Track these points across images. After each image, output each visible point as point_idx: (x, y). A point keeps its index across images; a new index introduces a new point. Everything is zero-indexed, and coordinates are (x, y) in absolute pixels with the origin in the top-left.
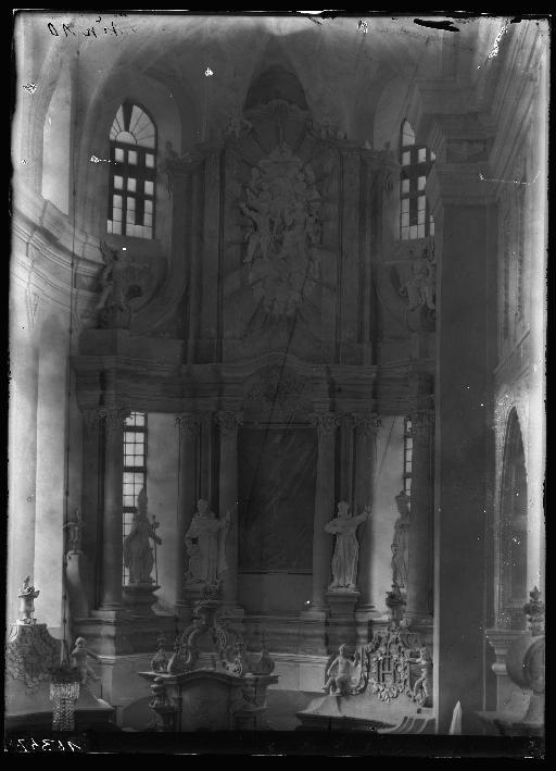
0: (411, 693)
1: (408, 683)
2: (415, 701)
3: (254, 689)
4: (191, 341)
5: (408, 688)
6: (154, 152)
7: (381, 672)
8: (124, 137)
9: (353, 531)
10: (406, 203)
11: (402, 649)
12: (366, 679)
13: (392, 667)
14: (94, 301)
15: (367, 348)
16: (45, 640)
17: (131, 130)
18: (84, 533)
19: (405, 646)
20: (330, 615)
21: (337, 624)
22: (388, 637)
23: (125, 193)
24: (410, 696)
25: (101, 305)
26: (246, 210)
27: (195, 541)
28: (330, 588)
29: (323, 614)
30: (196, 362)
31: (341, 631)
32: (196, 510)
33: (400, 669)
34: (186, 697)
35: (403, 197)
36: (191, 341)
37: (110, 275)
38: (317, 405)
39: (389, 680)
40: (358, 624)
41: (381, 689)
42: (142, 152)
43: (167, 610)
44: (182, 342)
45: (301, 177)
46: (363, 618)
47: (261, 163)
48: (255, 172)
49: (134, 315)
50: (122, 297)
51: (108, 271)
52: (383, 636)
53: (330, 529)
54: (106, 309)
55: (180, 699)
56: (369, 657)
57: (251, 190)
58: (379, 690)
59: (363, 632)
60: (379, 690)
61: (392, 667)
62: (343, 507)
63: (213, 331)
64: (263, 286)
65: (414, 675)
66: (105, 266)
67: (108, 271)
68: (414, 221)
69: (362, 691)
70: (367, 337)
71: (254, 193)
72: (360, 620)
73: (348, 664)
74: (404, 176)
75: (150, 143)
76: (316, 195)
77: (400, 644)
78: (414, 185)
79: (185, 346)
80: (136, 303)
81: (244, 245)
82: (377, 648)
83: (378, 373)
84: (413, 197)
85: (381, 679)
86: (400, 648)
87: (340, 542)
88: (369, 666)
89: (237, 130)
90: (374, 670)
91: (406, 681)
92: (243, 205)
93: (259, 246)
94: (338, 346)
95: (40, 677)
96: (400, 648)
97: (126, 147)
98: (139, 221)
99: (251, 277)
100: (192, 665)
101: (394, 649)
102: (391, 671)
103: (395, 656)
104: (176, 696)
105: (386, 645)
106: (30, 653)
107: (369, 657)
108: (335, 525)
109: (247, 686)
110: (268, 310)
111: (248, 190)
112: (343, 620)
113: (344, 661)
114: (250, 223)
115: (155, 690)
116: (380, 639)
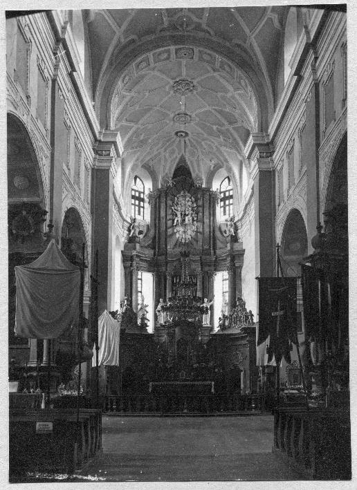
8: (135, 188)
15: (212, 251)
23: (135, 205)
39: (238, 322)
66: (131, 224)
74: (221, 201)
80: (141, 236)
81: (173, 220)
97: (135, 191)
98: (139, 214)
99: (175, 231)
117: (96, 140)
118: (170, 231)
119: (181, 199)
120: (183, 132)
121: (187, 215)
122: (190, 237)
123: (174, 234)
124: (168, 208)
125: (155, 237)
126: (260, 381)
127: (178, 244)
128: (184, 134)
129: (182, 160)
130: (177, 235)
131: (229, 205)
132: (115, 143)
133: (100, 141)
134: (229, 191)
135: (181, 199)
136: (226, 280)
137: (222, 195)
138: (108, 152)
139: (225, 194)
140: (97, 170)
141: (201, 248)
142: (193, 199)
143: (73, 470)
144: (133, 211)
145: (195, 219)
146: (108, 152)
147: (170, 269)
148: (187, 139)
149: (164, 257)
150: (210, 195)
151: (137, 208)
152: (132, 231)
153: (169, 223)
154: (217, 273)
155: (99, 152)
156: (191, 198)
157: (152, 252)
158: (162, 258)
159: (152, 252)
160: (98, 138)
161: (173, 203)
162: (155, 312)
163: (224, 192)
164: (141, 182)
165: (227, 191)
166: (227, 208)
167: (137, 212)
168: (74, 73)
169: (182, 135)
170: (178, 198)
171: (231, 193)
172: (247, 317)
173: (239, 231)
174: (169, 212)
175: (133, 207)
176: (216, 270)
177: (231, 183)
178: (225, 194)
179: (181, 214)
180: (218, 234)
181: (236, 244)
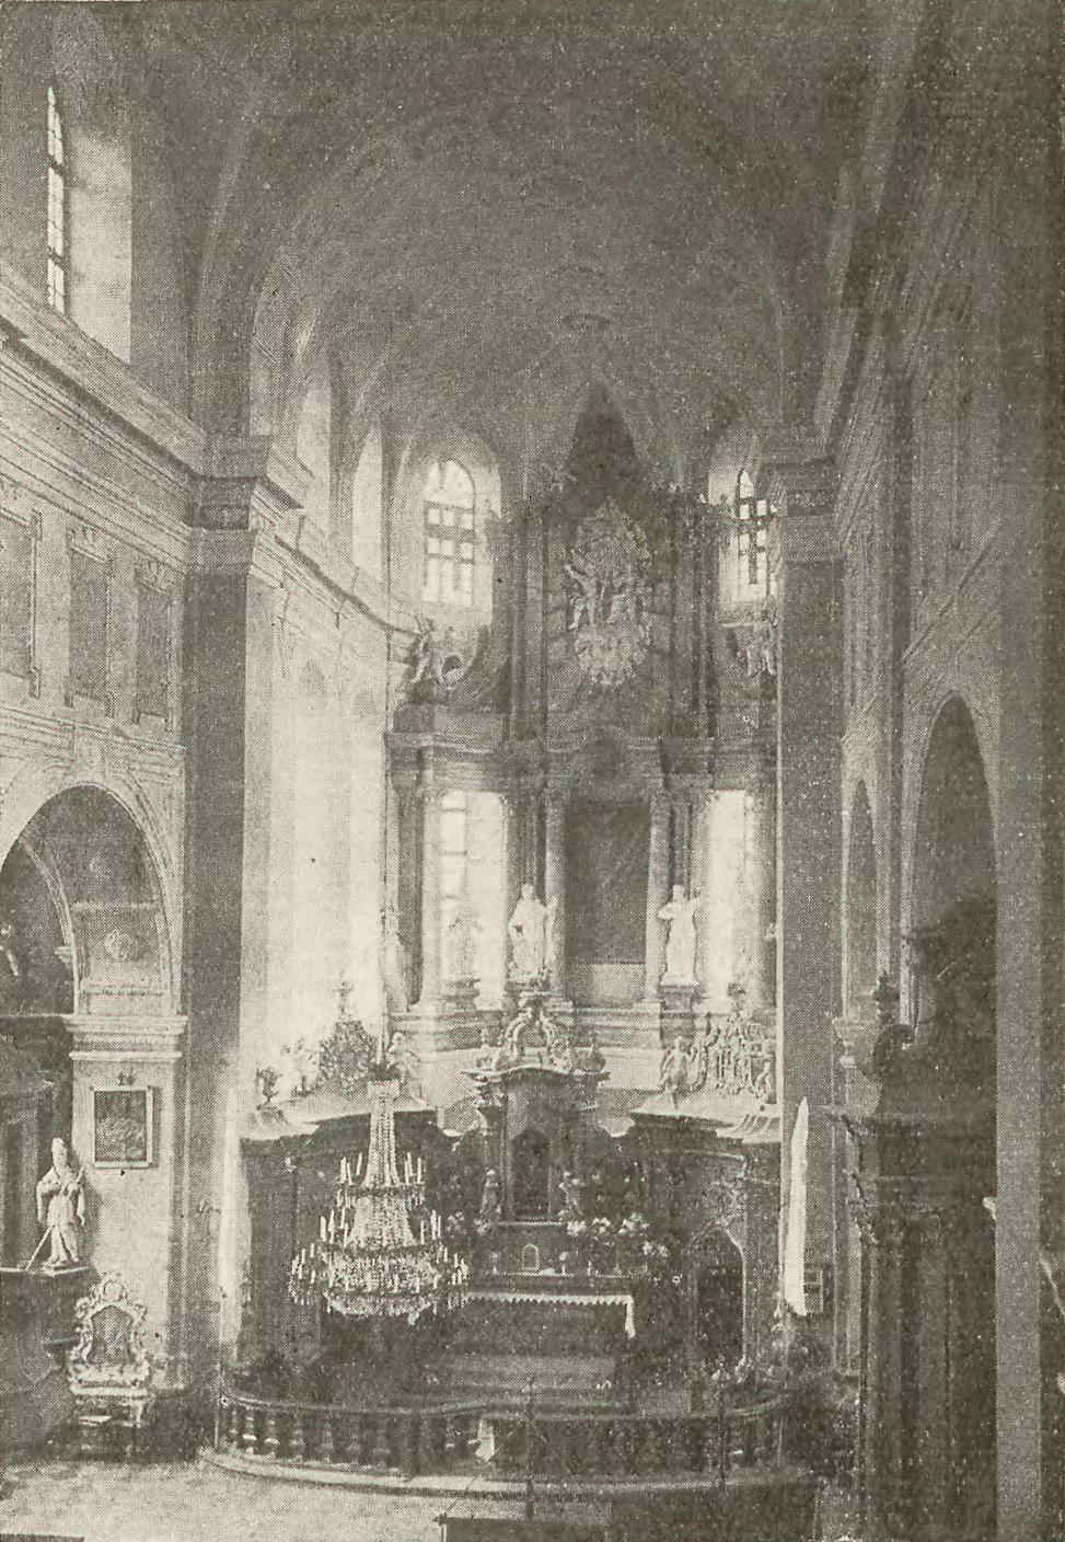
1: (749, 1078)
14: (410, 674)
27: (519, 929)
37: (426, 645)
42: (459, 511)
53: (663, 914)
55: (505, 1100)
76: (647, 555)
77: (741, 1036)
79: (507, 721)
80: (454, 675)
81: (569, 611)
102: (732, 1066)
107: (707, 1052)
129: (600, 394)
151: (449, 566)
170: (587, 530)
179: (599, 586)
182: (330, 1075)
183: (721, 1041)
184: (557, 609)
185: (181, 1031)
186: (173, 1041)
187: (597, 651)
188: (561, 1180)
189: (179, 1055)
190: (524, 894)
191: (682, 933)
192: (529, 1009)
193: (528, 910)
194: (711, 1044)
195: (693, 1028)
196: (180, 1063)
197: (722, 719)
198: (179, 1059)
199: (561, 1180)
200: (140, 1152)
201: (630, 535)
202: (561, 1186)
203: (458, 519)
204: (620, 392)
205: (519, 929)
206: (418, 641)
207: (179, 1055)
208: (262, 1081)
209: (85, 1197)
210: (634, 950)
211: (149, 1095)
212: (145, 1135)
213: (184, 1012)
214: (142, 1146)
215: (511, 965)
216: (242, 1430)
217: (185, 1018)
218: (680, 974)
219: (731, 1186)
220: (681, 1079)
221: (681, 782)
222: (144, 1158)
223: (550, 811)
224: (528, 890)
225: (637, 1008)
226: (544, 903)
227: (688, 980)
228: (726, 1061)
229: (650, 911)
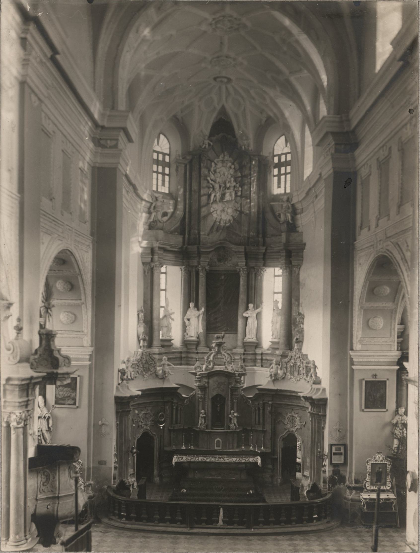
0: (306, 379)
1: (305, 374)
2: (308, 382)
3: (239, 377)
4: (187, 236)
5: (305, 377)
6: (169, 155)
7: (292, 370)
8: (157, 149)
9: (255, 315)
10: (276, 179)
11: (302, 361)
12: (285, 374)
13: (297, 368)
14: (149, 218)
15: (261, 239)
16: (151, 358)
17: (160, 145)
18: (145, 316)
19: (303, 359)
20: (245, 351)
21: (247, 354)
22: (295, 356)
23: (157, 172)
24: (306, 380)
25: (152, 220)
26: (210, 182)
27: (189, 320)
28: (245, 340)
29: (243, 350)
30: (189, 244)
31: (249, 357)
32: (190, 307)
33: (301, 369)
34: (211, 381)
35: (275, 176)
36: (187, 236)
37: (155, 207)
38: (239, 263)
39: (296, 373)
40: (255, 354)
41: (292, 377)
42: (164, 155)
43: (177, 348)
44: (182, 236)
45: (233, 167)
46: (258, 351)
47: (216, 161)
48: (213, 164)
49: (164, 224)
50: (159, 217)
51: (153, 205)
52: (293, 355)
53: (245, 315)
54: (153, 222)
55: (208, 383)
56: (286, 364)
57: (212, 172)
58: (291, 378)
59: (259, 357)
60: (291, 378)
61: (297, 368)
62: (251, 306)
63: (196, 232)
64: (216, 213)
65: (307, 371)
66: (152, 203)
67: (153, 205)
68: (279, 187)
69: (283, 378)
70: (261, 236)
71: (213, 174)
72: (257, 352)
73: (277, 367)
74: (275, 167)
75: (167, 151)
76: (239, 174)
77: (301, 359)
78: (279, 171)
79: (184, 238)
80: (166, 218)
81: (209, 196)
82: (290, 360)
83: (266, 250)
84: (279, 175)
85: (292, 373)
86: (301, 360)
87: (249, 321)
88: (286, 368)
89: (207, 146)
90: (289, 370)
91: (304, 374)
92: (209, 178)
93: (215, 196)
94: (249, 238)
95: (149, 374)
96: (301, 360)
97: (158, 153)
98: (163, 184)
99: (212, 210)
100: (213, 368)
101: (298, 361)
102: (297, 370)
103: (298, 364)
104: (206, 381)
105: (294, 359)
106: (145, 363)
107: (286, 364)
108: (247, 313)
109: (236, 376)
110: (218, 223)
111: (210, 172)
112: (251, 352)
113: (276, 366)
114: (211, 186)
115: (198, 378)
116: (292, 357)
117: (96, 124)
118: (204, 211)
119: (220, 165)
120: (225, 77)
121: (229, 188)
122: (231, 218)
123: (210, 214)
124: (202, 178)
125: (184, 218)
126: (324, 472)
127: (216, 228)
128: (225, 80)
129: (223, 111)
130: (215, 215)
131: (286, 174)
132: (125, 131)
133: (103, 127)
134: (286, 154)
135: (220, 165)
136: (279, 276)
137: (276, 160)
138: (114, 143)
139: (280, 159)
140: (99, 168)
141: (246, 235)
142: (237, 166)
143: (119, 1)
144: (154, 182)
145: (239, 194)
146: (114, 143)
147: (204, 262)
148: (229, 86)
149: (195, 247)
150: (259, 161)
151: (160, 176)
152: (154, 214)
153: (204, 199)
154: (266, 269)
155: (102, 142)
156: (233, 164)
157: (180, 239)
158: (194, 248)
159: (180, 239)
160: (100, 123)
161: (209, 171)
162: (183, 319)
163: (279, 156)
164: (166, 139)
165: (282, 154)
166: (283, 177)
167: (160, 183)
168: (58, 57)
169: (222, 82)
170: (216, 164)
171: (289, 157)
172: (308, 370)
173: (298, 216)
174: (204, 183)
175: (155, 175)
176: (265, 265)
177: (288, 145)
178: (280, 159)
179: (220, 186)
180: (269, 216)
181: (294, 235)
182: (140, 372)
183: (293, 361)
184: (204, 195)
185: (90, 353)
186: (88, 357)
187: (219, 212)
188: (230, 414)
189: (90, 363)
190: (191, 306)
191: (252, 323)
192: (217, 348)
193: (192, 313)
194: (288, 362)
195: (256, 359)
196: (90, 367)
197: (268, 240)
198: (90, 364)
199: (230, 414)
200: (73, 402)
201: (233, 167)
202: (230, 416)
203: (164, 158)
204: (230, 108)
205: (189, 320)
206: (151, 205)
207: (90, 363)
208: (120, 374)
209: (53, 420)
210: (233, 328)
211: (78, 379)
212: (76, 395)
213: (92, 346)
214: (74, 399)
215: (185, 334)
216: (120, 511)
217: (93, 348)
218: (251, 337)
219: (296, 416)
220: (276, 374)
221: (252, 264)
222: (75, 404)
223: (201, 274)
224: (192, 305)
225: (235, 351)
226: (198, 310)
227: (254, 340)
228: (294, 368)
229: (240, 313)
